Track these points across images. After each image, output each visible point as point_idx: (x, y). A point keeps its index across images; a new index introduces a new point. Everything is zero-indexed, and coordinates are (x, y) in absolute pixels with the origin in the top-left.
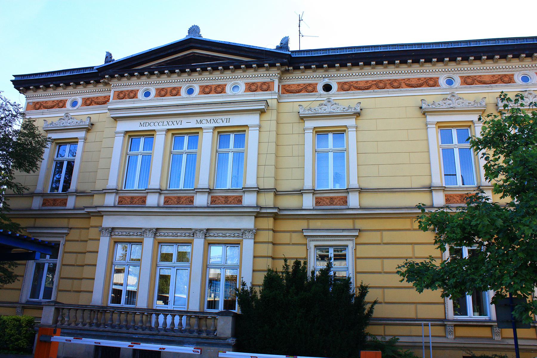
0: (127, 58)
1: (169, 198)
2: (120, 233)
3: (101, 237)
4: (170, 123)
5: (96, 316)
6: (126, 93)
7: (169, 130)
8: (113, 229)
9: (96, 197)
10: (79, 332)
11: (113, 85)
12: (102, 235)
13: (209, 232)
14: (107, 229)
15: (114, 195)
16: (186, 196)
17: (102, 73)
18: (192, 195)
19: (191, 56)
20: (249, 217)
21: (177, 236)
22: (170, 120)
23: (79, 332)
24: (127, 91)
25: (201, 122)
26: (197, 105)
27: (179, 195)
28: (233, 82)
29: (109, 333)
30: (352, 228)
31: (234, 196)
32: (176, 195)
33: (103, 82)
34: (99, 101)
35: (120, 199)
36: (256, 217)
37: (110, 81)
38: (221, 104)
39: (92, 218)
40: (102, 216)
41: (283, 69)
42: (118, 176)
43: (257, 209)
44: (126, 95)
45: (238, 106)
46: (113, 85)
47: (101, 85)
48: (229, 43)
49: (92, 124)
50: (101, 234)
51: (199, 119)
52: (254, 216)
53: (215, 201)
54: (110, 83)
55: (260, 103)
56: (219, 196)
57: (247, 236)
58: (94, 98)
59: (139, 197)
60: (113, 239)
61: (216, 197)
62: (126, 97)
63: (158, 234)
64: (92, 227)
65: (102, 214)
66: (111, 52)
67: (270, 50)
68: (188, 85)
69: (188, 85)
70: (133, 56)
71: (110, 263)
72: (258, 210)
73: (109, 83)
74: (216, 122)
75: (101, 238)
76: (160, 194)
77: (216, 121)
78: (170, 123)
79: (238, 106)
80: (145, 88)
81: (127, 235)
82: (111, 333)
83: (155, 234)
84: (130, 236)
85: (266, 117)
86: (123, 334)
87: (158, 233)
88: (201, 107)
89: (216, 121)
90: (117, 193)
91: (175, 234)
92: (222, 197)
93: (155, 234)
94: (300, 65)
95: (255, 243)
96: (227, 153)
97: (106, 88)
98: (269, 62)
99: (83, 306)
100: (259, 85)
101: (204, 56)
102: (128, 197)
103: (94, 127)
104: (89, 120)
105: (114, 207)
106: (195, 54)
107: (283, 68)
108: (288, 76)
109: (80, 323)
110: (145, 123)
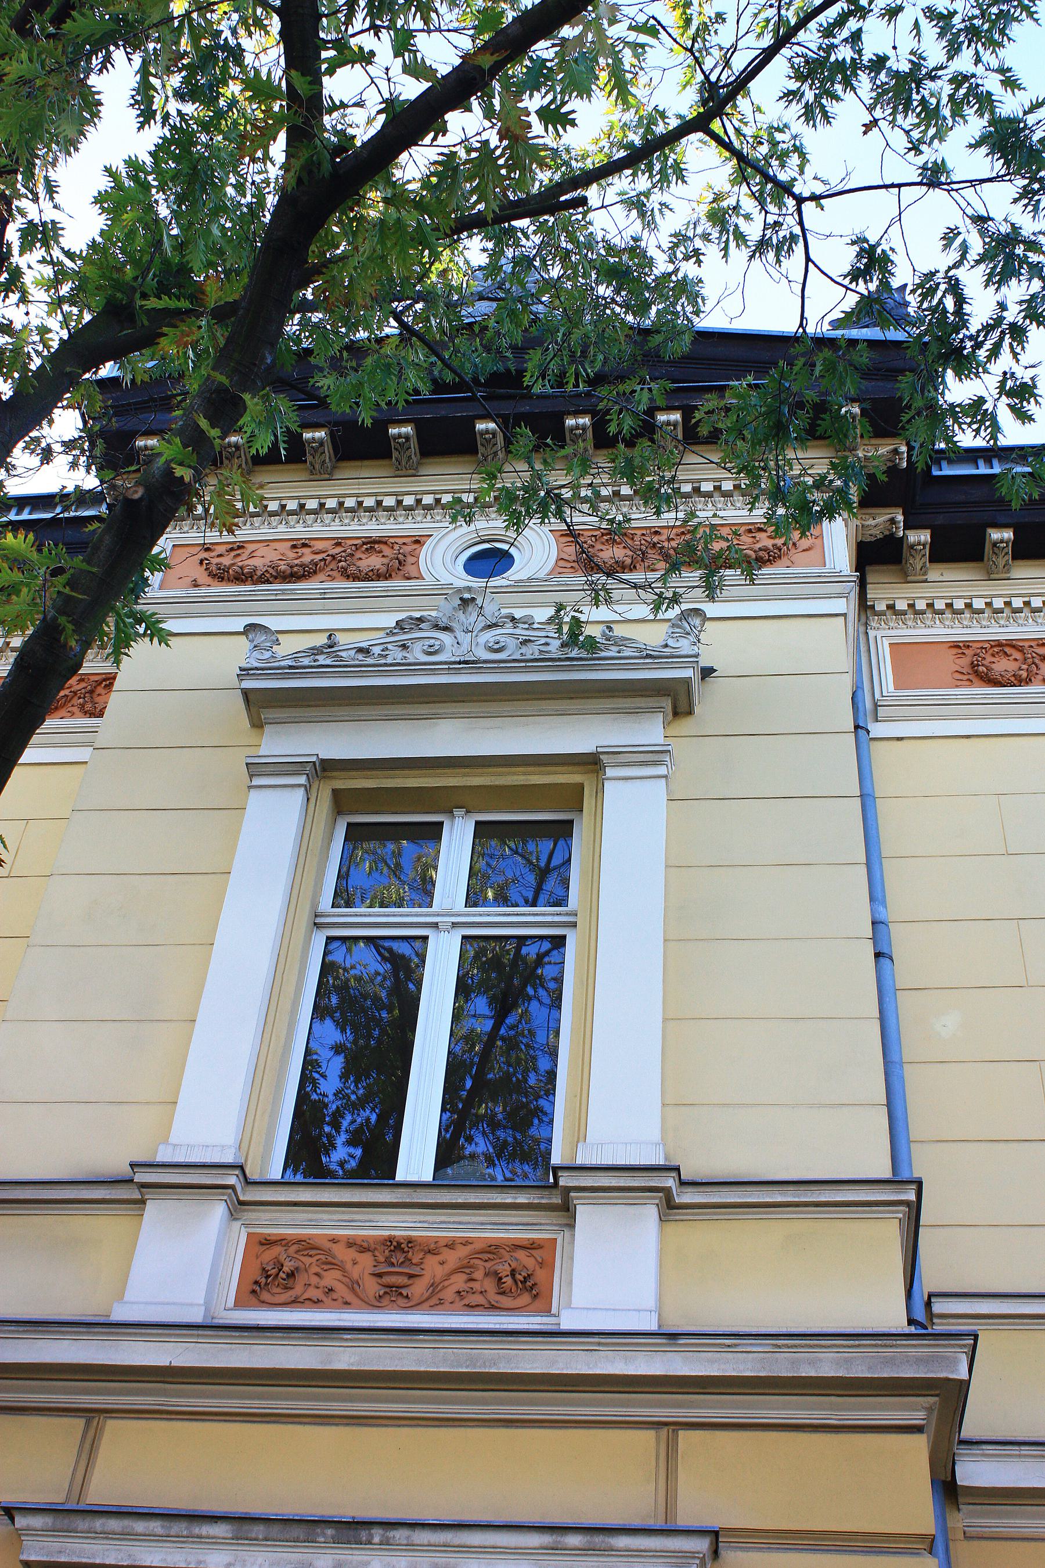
15: (218, 1210)
53: (291, 1275)
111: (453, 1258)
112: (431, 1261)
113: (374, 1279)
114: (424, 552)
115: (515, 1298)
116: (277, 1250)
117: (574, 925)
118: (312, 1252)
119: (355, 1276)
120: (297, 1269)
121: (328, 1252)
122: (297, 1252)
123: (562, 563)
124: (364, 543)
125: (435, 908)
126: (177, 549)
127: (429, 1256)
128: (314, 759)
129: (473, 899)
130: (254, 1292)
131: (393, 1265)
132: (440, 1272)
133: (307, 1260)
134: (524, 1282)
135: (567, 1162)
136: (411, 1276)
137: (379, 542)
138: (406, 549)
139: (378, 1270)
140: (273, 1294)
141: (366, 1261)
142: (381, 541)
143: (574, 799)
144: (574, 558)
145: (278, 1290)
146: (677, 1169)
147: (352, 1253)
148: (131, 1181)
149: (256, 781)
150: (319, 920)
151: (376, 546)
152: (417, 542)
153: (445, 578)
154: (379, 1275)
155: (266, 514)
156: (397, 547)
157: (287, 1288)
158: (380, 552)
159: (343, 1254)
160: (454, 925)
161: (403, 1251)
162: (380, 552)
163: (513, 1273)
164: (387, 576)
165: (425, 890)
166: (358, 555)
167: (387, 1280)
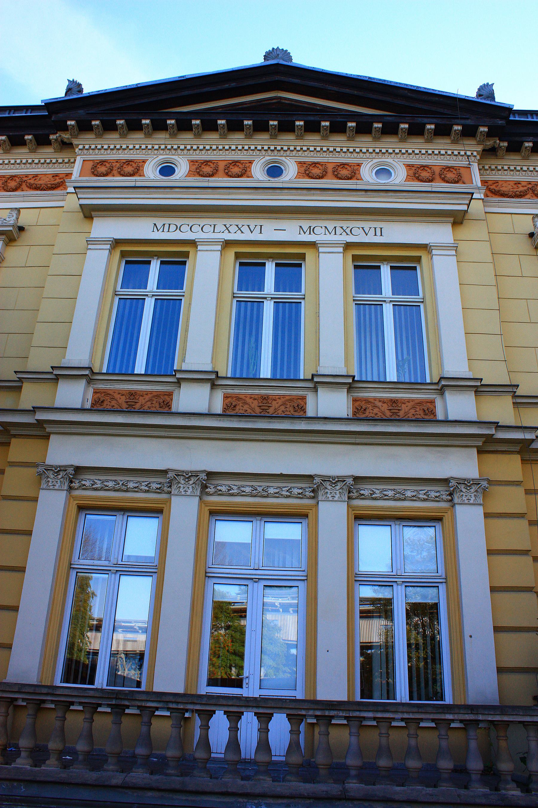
0: (125, 88)
1: (238, 398)
2: (99, 482)
3: (42, 492)
4: (233, 229)
5: (502, 738)
6: (114, 164)
7: (227, 244)
8: (78, 470)
9: (27, 387)
10: (23, 790)
11: (81, 147)
12: (44, 485)
13: (358, 486)
14: (59, 470)
15: (83, 383)
16: (284, 396)
17: (60, 115)
18: (301, 393)
19: (274, 103)
20: (463, 449)
21: (267, 497)
22: (233, 222)
23: (23, 790)
24: (117, 161)
25: (312, 230)
26: (305, 192)
27: (263, 392)
28: (375, 161)
29: (150, 794)
30: (116, 618)
31: (413, 401)
32: (257, 391)
33: (56, 140)
34: (40, 182)
35: (98, 395)
36: (480, 452)
37: (76, 137)
38: (363, 193)
39: (14, 441)
40: (47, 437)
41: (488, 143)
42: (95, 339)
43: (490, 428)
44: (115, 169)
45: (406, 201)
46: (81, 147)
47: (49, 150)
48: (369, 78)
49: (21, 229)
50: (43, 482)
51: (305, 224)
52: (477, 447)
53: (365, 410)
54: (75, 142)
55: (457, 199)
56: (375, 399)
57: (464, 498)
58: (27, 176)
59: (151, 392)
60: (75, 498)
61: (367, 401)
62: (115, 172)
63: (211, 490)
64: (13, 464)
65: (48, 430)
66: (79, 81)
67: (466, 98)
68: (268, 158)
69: (268, 158)
70: (139, 86)
71: (66, 564)
72: (492, 431)
73: (71, 144)
74: (349, 233)
75: (43, 495)
76: (214, 386)
77: (348, 231)
78: (233, 229)
79: (406, 201)
80: (161, 157)
81: (118, 490)
82: (157, 794)
83: (204, 487)
84: (127, 491)
85: (466, 232)
86: (205, 798)
87: (212, 487)
88: (314, 195)
89: (348, 231)
90: (90, 381)
91: (260, 489)
92: (383, 401)
93: (204, 487)
94: (524, 139)
95: (487, 515)
96: (379, 305)
97: (62, 156)
98: (463, 122)
99: (38, 690)
100: (437, 170)
101: (306, 105)
102: (121, 393)
103: (24, 235)
104: (15, 216)
105: (82, 410)
106: (283, 101)
107: (489, 141)
108: (493, 162)
109: (23, 754)
110: (167, 227)
111: (147, 398)
112: (403, 406)
113: (126, 403)
114: (146, 165)
115: (299, 413)
116: (229, 399)
117: (183, 296)
118: (108, 395)
119: (253, 407)
120: (104, 400)
121: (244, 400)
122: (236, 399)
123: (299, 174)
124: (126, 162)
125: (265, 292)
126: (85, 162)
127: (403, 404)
128: (223, 240)
129: (277, 289)
130: (224, 411)
131: (131, 399)
132: (277, 406)
133: (107, 398)
134: (301, 408)
135: (179, 369)
136: (136, 402)
137: (346, 165)
138: (356, 168)
139: (259, 405)
140: (360, 415)
141: (385, 405)
142: (210, 161)
143: (186, 255)
144: (303, 172)
145: (361, 414)
146: (217, 372)
147: (251, 400)
148: (52, 373)
149: (90, 247)
150: (235, 295)
151: (317, 165)
152: (143, 162)
153: (152, 177)
154: (127, 402)
155: (211, 150)
156: (352, 167)
157: (364, 413)
158: (318, 167)
159: (117, 396)
160: (272, 298)
161: (266, 400)
162: (105, 165)
163: (163, 402)
164: (350, 178)
165: (261, 287)
166: (203, 166)
167: (129, 403)
